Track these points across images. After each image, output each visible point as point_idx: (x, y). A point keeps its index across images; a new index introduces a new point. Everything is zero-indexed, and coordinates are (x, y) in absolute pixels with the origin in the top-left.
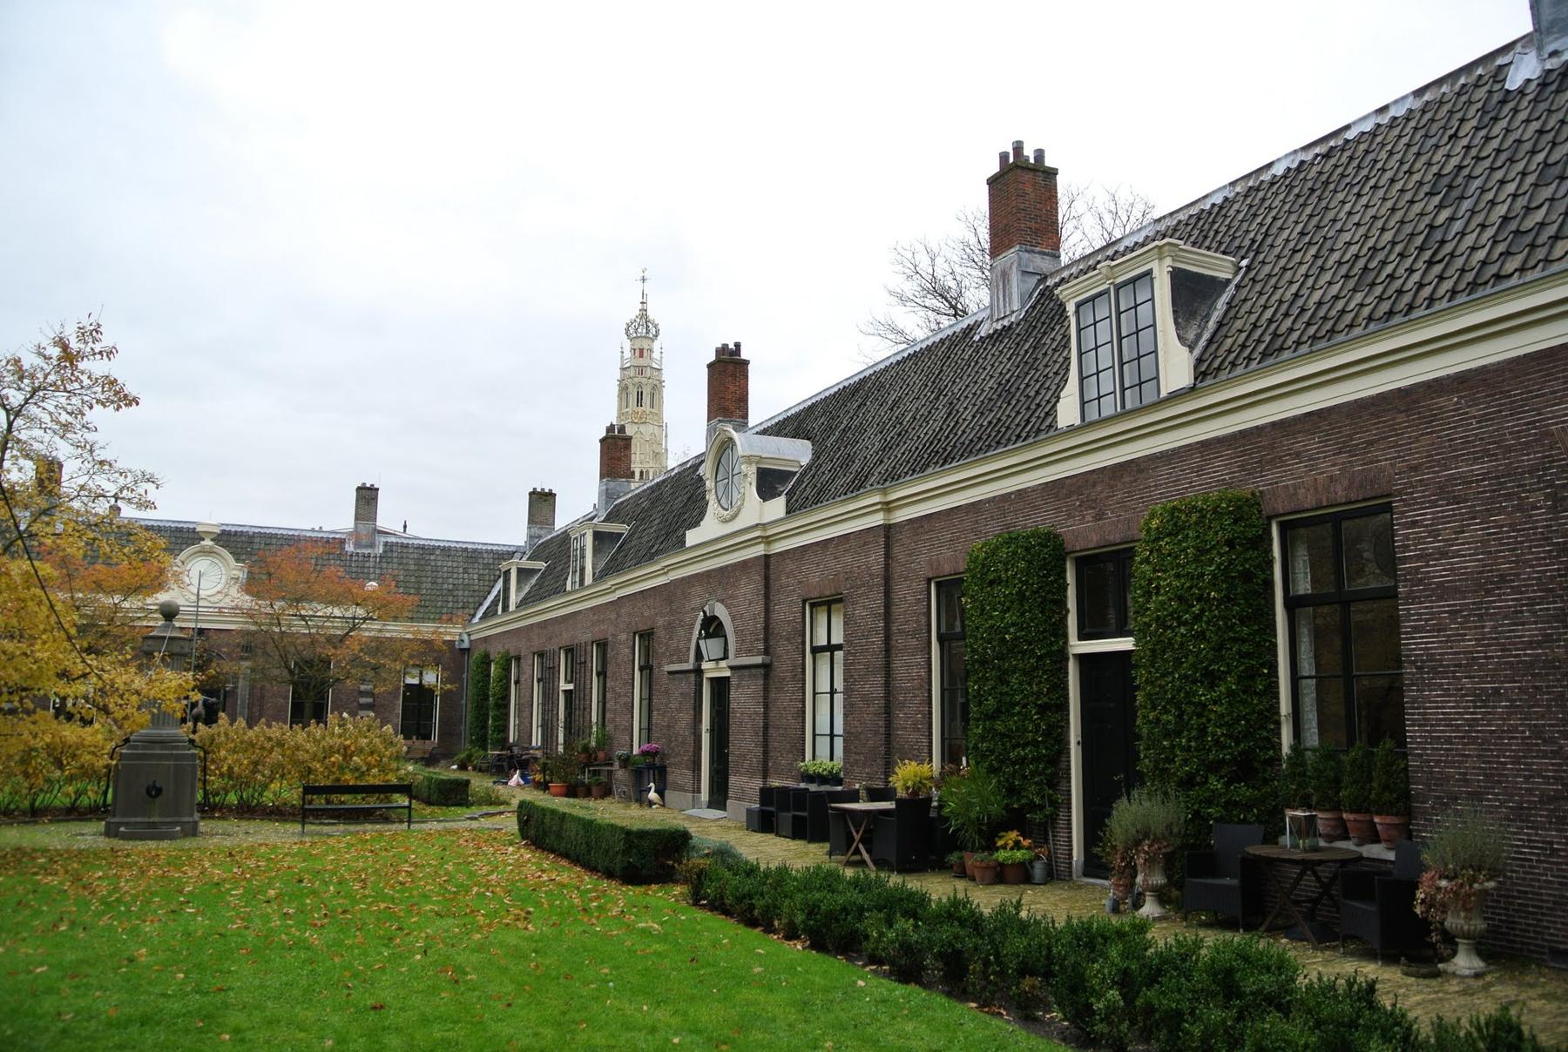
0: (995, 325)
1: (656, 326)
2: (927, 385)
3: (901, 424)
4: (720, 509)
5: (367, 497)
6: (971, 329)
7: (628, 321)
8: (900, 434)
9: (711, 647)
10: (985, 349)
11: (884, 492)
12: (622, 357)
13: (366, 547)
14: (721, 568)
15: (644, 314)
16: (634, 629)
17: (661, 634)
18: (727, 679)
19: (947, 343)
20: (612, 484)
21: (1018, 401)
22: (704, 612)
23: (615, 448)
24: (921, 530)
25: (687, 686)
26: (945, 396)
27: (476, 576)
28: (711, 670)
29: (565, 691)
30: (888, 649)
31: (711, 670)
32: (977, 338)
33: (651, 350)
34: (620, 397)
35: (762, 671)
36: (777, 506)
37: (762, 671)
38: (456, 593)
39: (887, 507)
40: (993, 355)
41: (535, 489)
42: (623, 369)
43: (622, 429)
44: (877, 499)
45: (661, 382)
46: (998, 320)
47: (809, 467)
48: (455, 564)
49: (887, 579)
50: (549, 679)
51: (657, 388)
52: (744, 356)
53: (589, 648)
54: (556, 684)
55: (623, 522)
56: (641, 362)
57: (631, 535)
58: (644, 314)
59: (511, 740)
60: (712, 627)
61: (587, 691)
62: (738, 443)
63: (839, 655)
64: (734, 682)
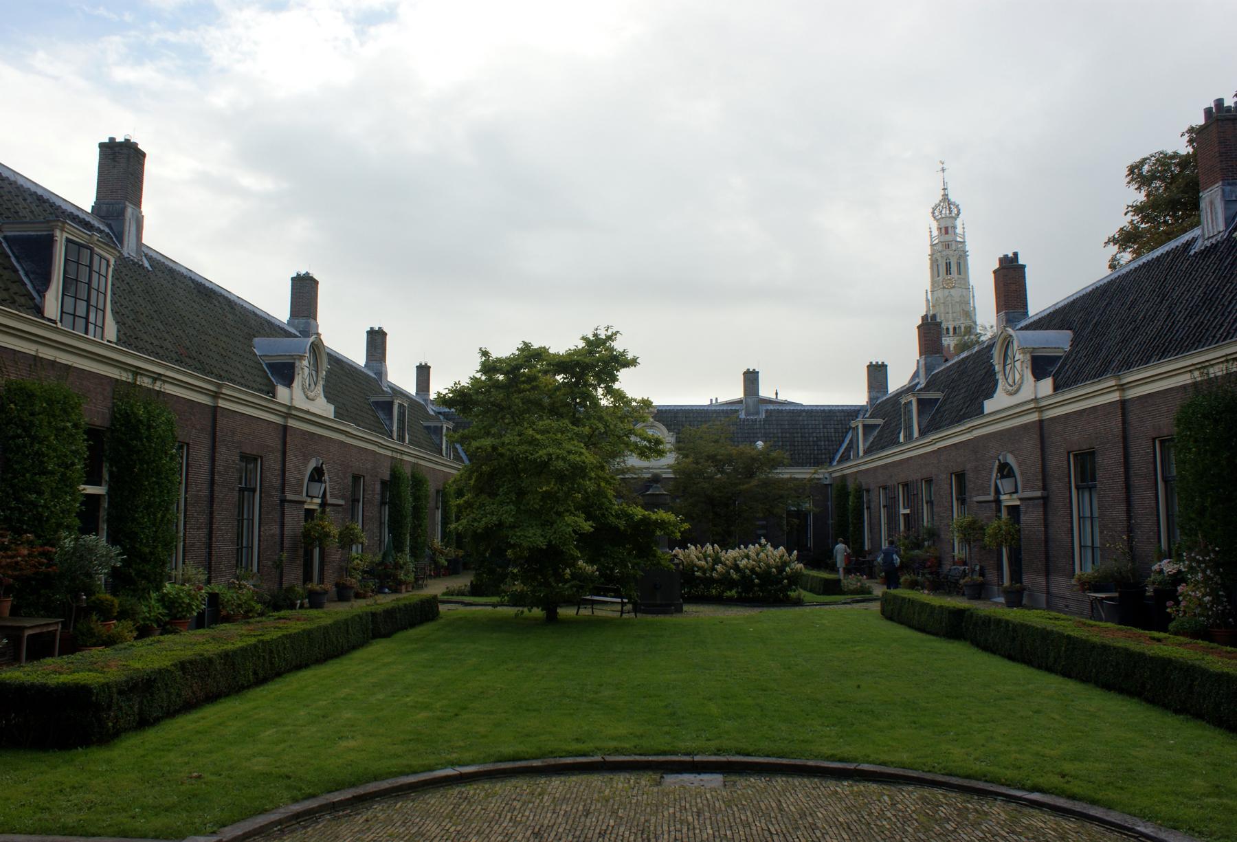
0: (1206, 242)
1: (957, 206)
2: (1155, 291)
3: (1135, 321)
4: (1007, 385)
5: (751, 378)
6: (1189, 245)
8: (1134, 330)
9: (1005, 485)
10: (1198, 263)
11: (1118, 378)
13: (753, 414)
15: (945, 198)
16: (951, 471)
17: (970, 475)
18: (1018, 506)
19: (1171, 255)
20: (929, 359)
21: (1217, 308)
22: (999, 460)
23: (930, 331)
24: (1146, 404)
26: (1167, 300)
27: (833, 430)
28: (1008, 500)
29: (904, 514)
30: (1128, 487)
31: (1008, 500)
32: (1192, 253)
33: (955, 227)
34: (932, 268)
35: (1041, 501)
36: (1046, 386)
37: (1041, 501)
38: (819, 443)
39: (1122, 388)
40: (1203, 268)
41: (871, 363)
42: (932, 245)
43: (934, 317)
44: (1113, 383)
46: (1209, 238)
47: (1070, 353)
48: (817, 423)
49: (1125, 438)
50: (891, 507)
52: (1021, 262)
55: (938, 390)
56: (948, 238)
57: (945, 400)
58: (945, 198)
59: (866, 548)
60: (1005, 471)
61: (920, 515)
62: (1015, 338)
64: (1023, 509)
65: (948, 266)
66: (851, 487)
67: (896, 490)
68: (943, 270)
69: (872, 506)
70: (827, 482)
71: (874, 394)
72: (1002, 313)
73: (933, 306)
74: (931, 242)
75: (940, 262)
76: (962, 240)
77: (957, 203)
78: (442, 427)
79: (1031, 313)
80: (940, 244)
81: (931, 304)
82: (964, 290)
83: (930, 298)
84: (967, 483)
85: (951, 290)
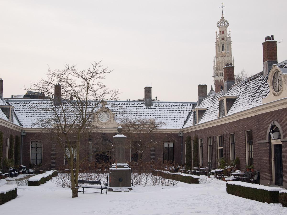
1: (227, 22)
7: (218, 22)
12: (216, 34)
14: (276, 111)
15: (223, 19)
18: (281, 145)
20: (229, 82)
25: (266, 148)
29: (276, 146)
31: (274, 142)
33: (226, 31)
42: (217, 38)
45: (230, 41)
51: (230, 43)
53: (228, 136)
54: (216, 147)
56: (223, 35)
58: (223, 19)
60: (274, 129)
61: (228, 149)
63: (211, 138)
64: (283, 146)
65: (223, 47)
66: (193, 137)
67: (216, 138)
68: (221, 49)
69: (203, 146)
70: (181, 135)
71: (201, 98)
72: (266, 62)
73: (217, 64)
74: (217, 37)
75: (220, 45)
76: (229, 37)
77: (228, 21)
78: (9, 108)
79: (279, 62)
80: (220, 38)
81: (215, 63)
82: (229, 57)
83: (215, 60)
84: (253, 135)
85: (224, 57)
